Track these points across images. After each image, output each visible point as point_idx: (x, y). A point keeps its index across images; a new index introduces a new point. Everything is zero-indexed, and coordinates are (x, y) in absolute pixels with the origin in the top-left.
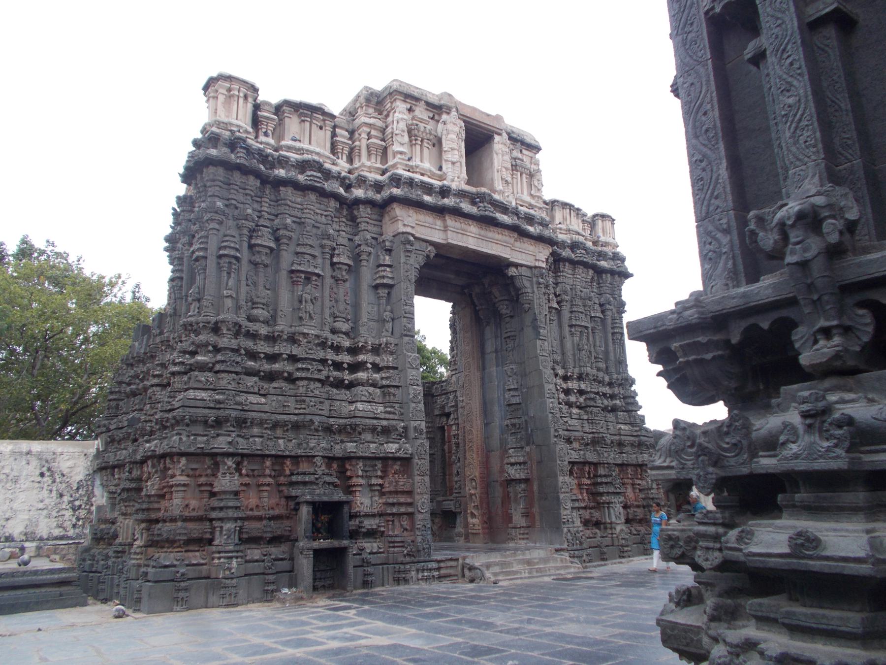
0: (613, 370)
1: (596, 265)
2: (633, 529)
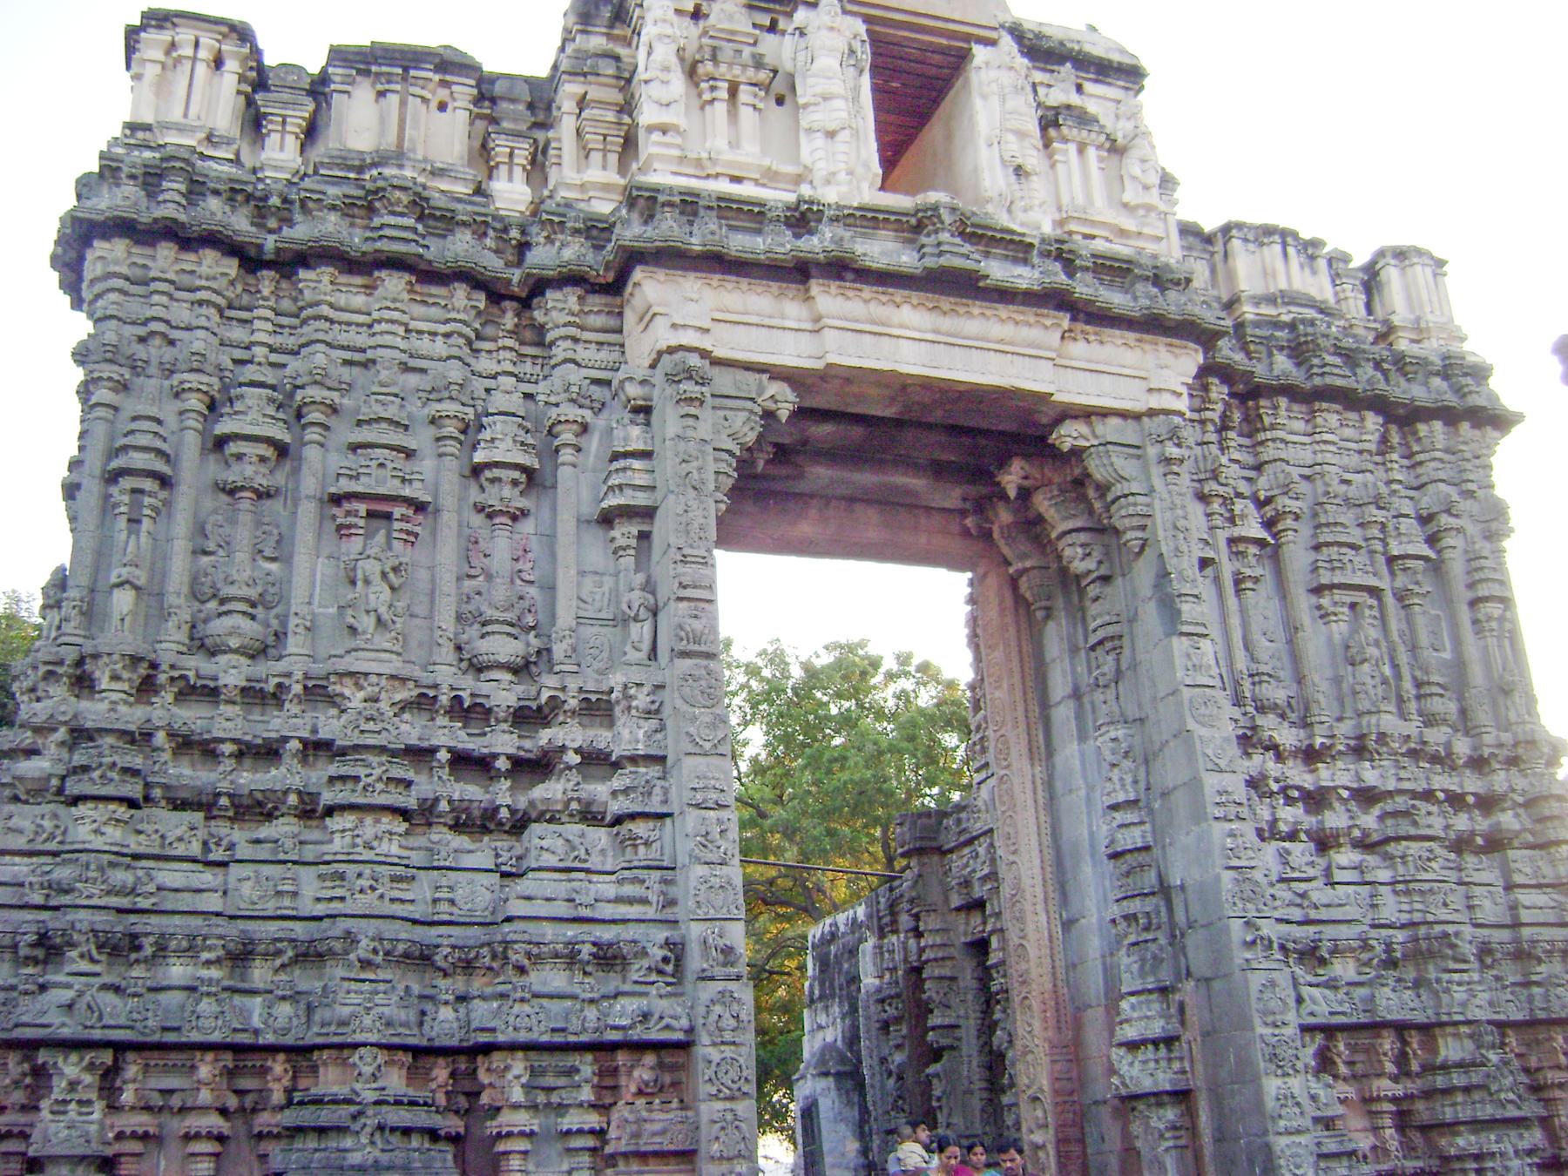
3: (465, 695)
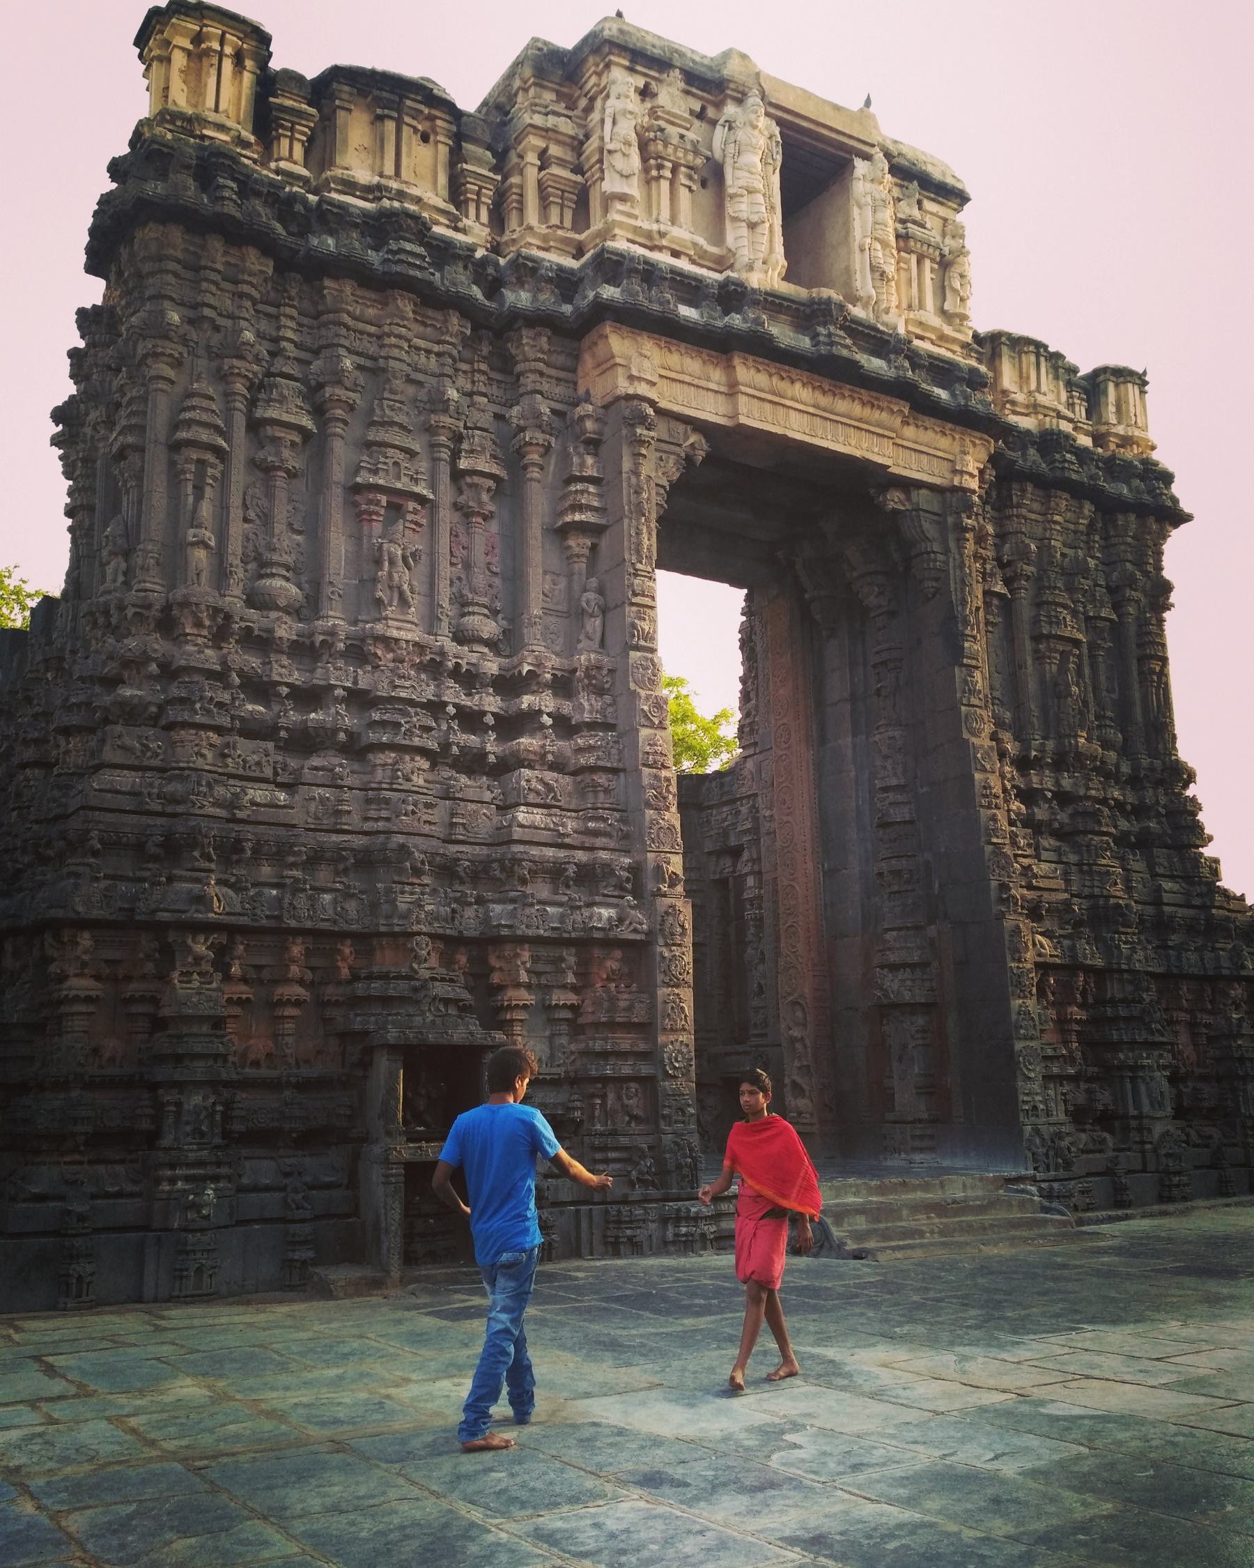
1: (1102, 491)
2: (1192, 1133)
3: (463, 663)
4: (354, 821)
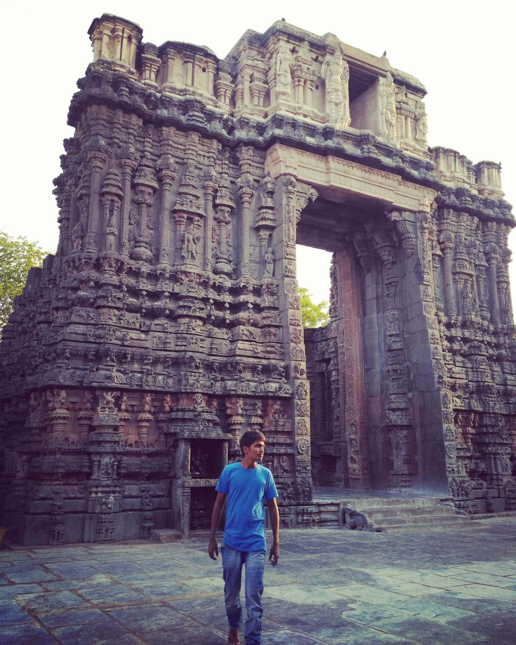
0: (498, 319)
3: (217, 282)
4: (172, 346)
